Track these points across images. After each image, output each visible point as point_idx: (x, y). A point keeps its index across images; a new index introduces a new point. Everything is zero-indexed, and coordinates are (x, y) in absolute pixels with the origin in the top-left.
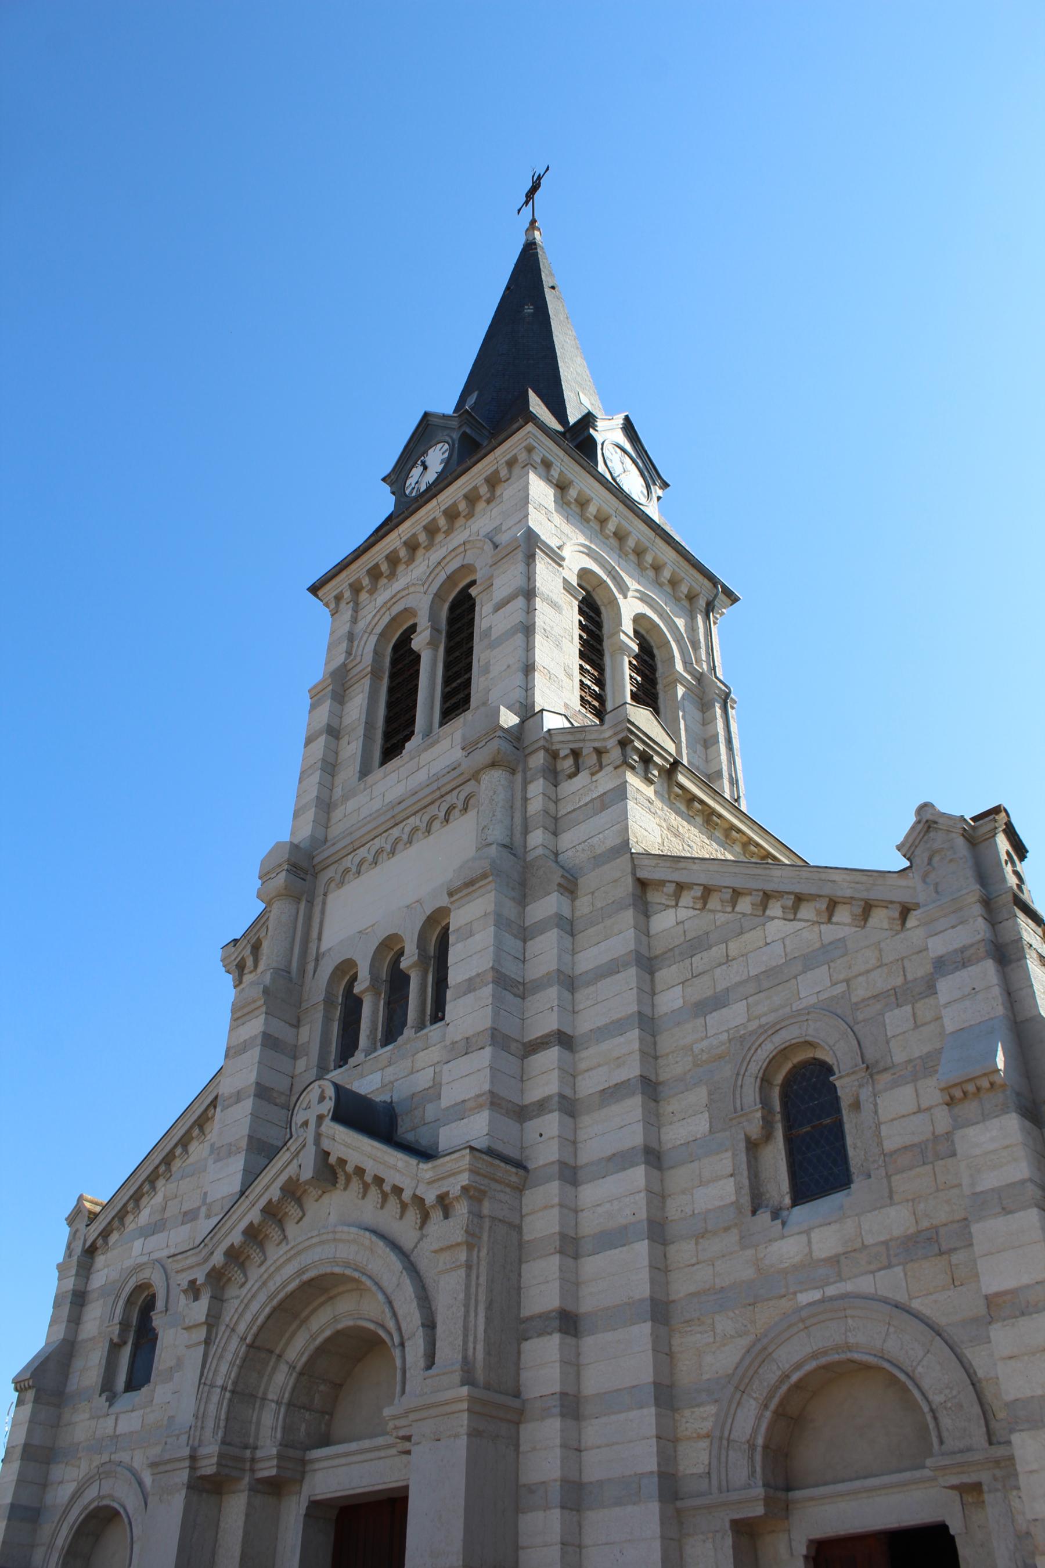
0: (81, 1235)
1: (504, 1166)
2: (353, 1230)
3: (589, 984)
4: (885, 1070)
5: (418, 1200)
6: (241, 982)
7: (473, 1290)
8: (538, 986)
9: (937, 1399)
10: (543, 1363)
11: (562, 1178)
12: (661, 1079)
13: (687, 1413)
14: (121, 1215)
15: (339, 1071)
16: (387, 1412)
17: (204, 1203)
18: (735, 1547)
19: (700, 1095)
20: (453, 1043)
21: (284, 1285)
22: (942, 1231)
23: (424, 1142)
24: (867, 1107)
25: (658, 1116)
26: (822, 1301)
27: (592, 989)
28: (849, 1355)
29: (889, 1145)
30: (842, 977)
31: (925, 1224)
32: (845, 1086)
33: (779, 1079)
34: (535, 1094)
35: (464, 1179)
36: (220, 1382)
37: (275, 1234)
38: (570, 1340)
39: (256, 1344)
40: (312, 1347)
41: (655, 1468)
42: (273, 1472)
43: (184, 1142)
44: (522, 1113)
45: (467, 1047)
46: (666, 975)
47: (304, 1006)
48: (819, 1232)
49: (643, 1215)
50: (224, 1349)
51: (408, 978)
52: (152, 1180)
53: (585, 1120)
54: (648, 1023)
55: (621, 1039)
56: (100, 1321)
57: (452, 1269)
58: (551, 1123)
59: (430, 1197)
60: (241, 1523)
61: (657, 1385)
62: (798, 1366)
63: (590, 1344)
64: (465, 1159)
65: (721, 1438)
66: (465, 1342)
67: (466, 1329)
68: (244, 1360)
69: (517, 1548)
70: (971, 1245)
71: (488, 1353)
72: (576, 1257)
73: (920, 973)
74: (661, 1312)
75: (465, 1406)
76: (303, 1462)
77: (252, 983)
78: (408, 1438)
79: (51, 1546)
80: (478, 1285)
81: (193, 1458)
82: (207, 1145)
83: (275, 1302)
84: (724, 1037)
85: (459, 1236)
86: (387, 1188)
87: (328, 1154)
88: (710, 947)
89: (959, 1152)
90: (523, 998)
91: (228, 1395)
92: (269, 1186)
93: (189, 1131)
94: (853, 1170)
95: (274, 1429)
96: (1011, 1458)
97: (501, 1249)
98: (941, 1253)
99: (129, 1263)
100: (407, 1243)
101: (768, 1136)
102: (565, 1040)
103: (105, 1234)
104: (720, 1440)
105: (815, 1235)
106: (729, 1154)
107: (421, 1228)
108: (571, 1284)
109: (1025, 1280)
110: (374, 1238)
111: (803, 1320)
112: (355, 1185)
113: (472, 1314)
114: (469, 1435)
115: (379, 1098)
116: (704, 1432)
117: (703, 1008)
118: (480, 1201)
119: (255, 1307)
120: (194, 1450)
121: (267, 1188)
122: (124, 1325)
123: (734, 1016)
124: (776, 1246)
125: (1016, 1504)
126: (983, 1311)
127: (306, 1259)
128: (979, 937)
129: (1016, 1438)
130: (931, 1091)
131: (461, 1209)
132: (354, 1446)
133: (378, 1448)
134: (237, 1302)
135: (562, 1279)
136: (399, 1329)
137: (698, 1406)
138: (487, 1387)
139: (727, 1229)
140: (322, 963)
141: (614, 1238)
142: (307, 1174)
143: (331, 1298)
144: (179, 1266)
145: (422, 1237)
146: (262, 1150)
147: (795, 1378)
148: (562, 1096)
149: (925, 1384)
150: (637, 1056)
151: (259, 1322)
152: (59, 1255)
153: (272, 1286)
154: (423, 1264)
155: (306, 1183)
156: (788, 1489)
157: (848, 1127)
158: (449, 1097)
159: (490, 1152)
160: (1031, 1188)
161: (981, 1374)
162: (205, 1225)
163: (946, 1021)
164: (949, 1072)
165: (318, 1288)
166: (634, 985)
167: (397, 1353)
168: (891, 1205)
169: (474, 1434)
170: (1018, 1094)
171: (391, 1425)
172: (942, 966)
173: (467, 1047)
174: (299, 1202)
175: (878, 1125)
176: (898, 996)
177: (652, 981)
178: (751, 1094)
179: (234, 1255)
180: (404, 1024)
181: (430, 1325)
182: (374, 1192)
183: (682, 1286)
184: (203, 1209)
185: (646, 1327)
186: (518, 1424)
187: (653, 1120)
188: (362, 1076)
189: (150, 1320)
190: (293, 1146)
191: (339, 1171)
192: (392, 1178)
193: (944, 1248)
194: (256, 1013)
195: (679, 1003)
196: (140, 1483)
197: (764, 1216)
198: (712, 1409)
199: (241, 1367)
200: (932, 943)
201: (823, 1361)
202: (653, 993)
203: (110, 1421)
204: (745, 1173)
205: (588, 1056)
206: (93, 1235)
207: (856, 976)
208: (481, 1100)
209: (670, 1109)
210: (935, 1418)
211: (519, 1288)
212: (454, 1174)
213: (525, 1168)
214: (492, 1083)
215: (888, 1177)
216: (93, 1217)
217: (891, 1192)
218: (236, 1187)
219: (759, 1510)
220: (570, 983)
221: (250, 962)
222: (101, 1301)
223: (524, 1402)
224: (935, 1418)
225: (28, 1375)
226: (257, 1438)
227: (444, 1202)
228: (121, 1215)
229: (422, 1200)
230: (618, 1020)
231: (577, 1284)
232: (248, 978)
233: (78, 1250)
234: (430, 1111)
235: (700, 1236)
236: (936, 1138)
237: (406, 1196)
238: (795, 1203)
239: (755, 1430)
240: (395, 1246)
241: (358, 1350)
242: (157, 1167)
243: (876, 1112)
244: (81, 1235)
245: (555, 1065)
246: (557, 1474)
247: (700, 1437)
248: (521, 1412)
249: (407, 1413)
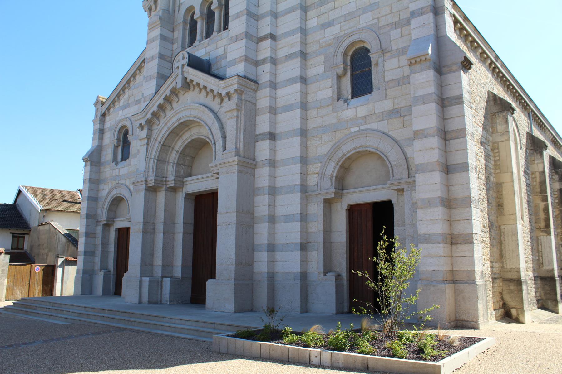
0: (99, 110)
1: (250, 82)
2: (197, 105)
3: (282, 16)
4: (389, 52)
5: (219, 94)
6: (150, 15)
7: (239, 125)
8: (263, 16)
9: (393, 163)
10: (263, 150)
11: (271, 87)
12: (308, 52)
13: (311, 166)
14: (113, 102)
15: (189, 48)
16: (210, 165)
17: (143, 97)
18: (324, 207)
19: (321, 58)
20: (232, 37)
21: (173, 124)
22: (402, 109)
23: (221, 74)
24: (381, 65)
25: (306, 65)
26: (359, 131)
27: (283, 18)
28: (366, 149)
29: (387, 79)
30: (376, 17)
31: (396, 107)
32: (374, 57)
33: (350, 53)
34: (261, 57)
35: (236, 87)
36: (153, 157)
37: (169, 107)
38: (272, 142)
39: (165, 144)
40: (184, 145)
41: (300, 183)
42: (173, 185)
43: (134, 76)
44: (256, 64)
45: (237, 39)
46: (311, 13)
47: (175, 24)
48: (361, 107)
49: (299, 100)
50: (153, 146)
51: (214, 13)
52: (123, 89)
53: (280, 66)
54: (304, 31)
55: (294, 37)
56: (110, 139)
57: (231, 118)
58: (267, 67)
59: (224, 93)
60: (164, 200)
61: (301, 157)
62: (349, 152)
63: (279, 143)
64: (236, 79)
65: (322, 174)
66: (236, 142)
67: (236, 138)
68: (161, 149)
69: (254, 207)
70: (411, 114)
71: (244, 146)
72: (275, 114)
73: (405, 17)
74: (304, 133)
75: (236, 163)
76: (183, 182)
77: (155, 15)
78: (217, 174)
79: (103, 208)
80: (241, 123)
81: (146, 181)
82: (142, 77)
83: (170, 130)
84: (331, 37)
85: (234, 107)
86: (208, 90)
87: (186, 78)
88: (328, 3)
89: (411, 82)
90: (258, 21)
91: (156, 161)
92: (166, 90)
93: (135, 72)
94: (374, 87)
95: (172, 171)
96: (414, 182)
97: (249, 112)
98: (401, 116)
99: (118, 119)
100: (216, 110)
101: (345, 74)
102: (273, 37)
103: (108, 109)
104: (322, 175)
105: (358, 109)
106: (330, 80)
107: (221, 104)
108: (273, 123)
109: (428, 126)
110: (204, 108)
111: (352, 137)
112: (197, 89)
113: (239, 133)
114: (238, 172)
115: (204, 58)
117: (324, 26)
118: (241, 94)
119: (163, 132)
120: (146, 178)
121: (165, 91)
122: (118, 140)
123: (336, 30)
124: (345, 112)
125: (414, 194)
126: (412, 136)
127: (180, 115)
128: (429, 4)
129: (417, 175)
130: (404, 61)
131: (235, 97)
132: (199, 177)
133: (207, 177)
134: (157, 131)
135: (270, 122)
136: (214, 138)
138: (244, 157)
139: (328, 106)
140: (181, 7)
141: (289, 108)
142: (179, 85)
144: (136, 119)
145: (221, 107)
146: (162, 78)
147: (347, 156)
148: (271, 58)
149: (390, 159)
150: (299, 43)
151: (165, 137)
152: (93, 117)
153: (169, 125)
154: (221, 117)
155: (179, 89)
156: (343, 190)
157: (373, 72)
158: (230, 57)
159: (245, 77)
160: (434, 96)
161: (409, 156)
162: (144, 105)
163: (413, 35)
164: (411, 54)
165: (185, 125)
166: (299, 17)
167: (213, 146)
168: (386, 99)
169: (239, 172)
170: (434, 63)
171: (212, 169)
172: (413, 14)
173: (237, 39)
174: (177, 95)
175: (384, 71)
176: (396, 25)
177: (306, 15)
178: (340, 59)
179: (154, 114)
180: (213, 30)
181: (224, 137)
182: (203, 92)
183: (311, 125)
184: (143, 99)
185: (299, 138)
186: (254, 169)
187: (304, 67)
188: (198, 50)
189: (127, 138)
190: (174, 75)
191: (191, 84)
192: (210, 86)
193: (402, 114)
194: (157, 27)
195: (316, 24)
196: (129, 189)
197: (341, 102)
198: (319, 165)
199: (160, 152)
200: (411, 5)
201: (358, 150)
202: (306, 20)
203: (117, 171)
204: (336, 87)
205: (281, 43)
206: (104, 110)
208: (242, 58)
209: (310, 63)
210: (392, 169)
211: (255, 125)
212: (232, 85)
213: (258, 83)
214: (246, 52)
215: (386, 90)
216: (103, 103)
217: (386, 95)
218: (154, 91)
219: (333, 196)
220: (275, 15)
221: (153, 7)
222: (109, 132)
223: (256, 162)
224: (392, 169)
225: (87, 157)
226: (167, 174)
227: (228, 95)
228: (113, 102)
229: (221, 94)
230: (293, 30)
231: (275, 124)
232: (153, 14)
233: (99, 115)
234: (223, 63)
235: (318, 108)
236: (404, 77)
237: (215, 93)
238: (352, 98)
239: (333, 172)
240: (212, 110)
241: (200, 146)
242: (125, 85)
243: (384, 67)
244: (99, 110)
245: (269, 46)
246: (267, 184)
247: (315, 174)
248: (256, 165)
249: (217, 166)
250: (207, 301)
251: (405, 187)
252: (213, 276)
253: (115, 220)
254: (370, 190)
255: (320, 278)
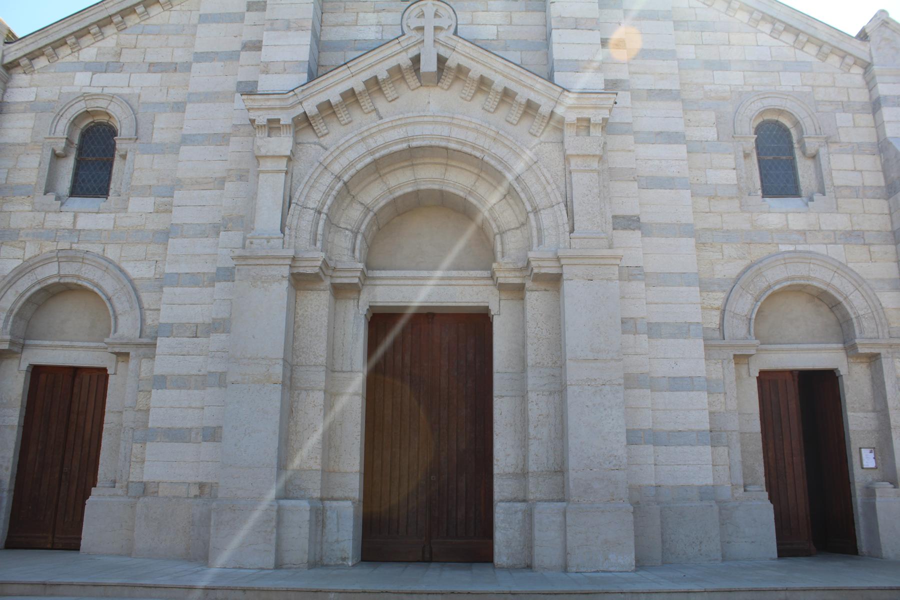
4: (836, 142)
26: (795, 251)
32: (121, 146)
62: (777, 283)
98: (864, 244)
106: (732, 156)
111: (784, 259)
116: (716, 306)
137: (712, 291)
139: (731, 198)
143: (413, 165)
193: (867, 241)
197: (51, 197)
207: (819, 86)
235: (712, 198)
250: (83, 543)
251: (883, 351)
252: (95, 486)
253: (28, 342)
254: (802, 350)
255: (736, 495)
